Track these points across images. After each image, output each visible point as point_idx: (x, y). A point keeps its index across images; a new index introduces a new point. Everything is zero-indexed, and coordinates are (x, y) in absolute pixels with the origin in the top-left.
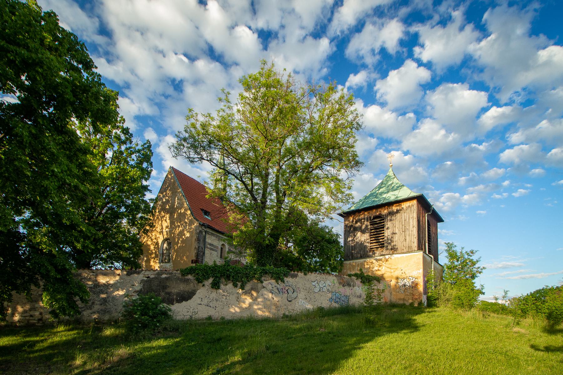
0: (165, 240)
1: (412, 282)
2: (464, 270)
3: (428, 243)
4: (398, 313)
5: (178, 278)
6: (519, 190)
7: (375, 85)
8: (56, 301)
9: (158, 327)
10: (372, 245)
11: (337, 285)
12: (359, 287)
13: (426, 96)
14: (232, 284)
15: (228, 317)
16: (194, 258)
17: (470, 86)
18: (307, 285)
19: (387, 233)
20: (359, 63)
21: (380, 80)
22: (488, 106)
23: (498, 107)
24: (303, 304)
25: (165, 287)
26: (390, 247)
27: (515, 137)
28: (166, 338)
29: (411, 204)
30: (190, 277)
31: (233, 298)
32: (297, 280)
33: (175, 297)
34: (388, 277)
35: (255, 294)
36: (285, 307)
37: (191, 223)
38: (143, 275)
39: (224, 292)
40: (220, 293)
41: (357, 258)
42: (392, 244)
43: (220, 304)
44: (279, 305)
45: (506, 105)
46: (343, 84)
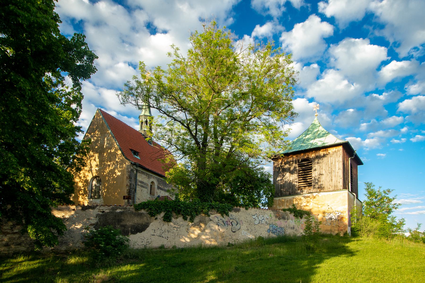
0: (94, 178)
1: (338, 216)
2: (380, 206)
3: (351, 183)
4: (332, 242)
5: (132, 213)
6: (417, 136)
7: (280, 36)
8: (43, 232)
9: (120, 255)
10: (300, 184)
11: (274, 218)
12: (292, 220)
13: (330, 48)
14: (182, 217)
15: (179, 246)
16: (126, 195)
17: (371, 41)
18: (248, 218)
19: (314, 174)
20: (264, 15)
21: (285, 32)
22: (388, 60)
23: (397, 61)
24: (246, 234)
25: (120, 221)
26: (317, 186)
27: (413, 89)
28: (131, 264)
29: (337, 150)
30: (143, 211)
31: (184, 229)
32: (239, 214)
33: (130, 229)
34: (316, 212)
35: (203, 225)
36: (230, 237)
37: (122, 162)
38: (98, 210)
39: (175, 224)
40: (171, 225)
41: (286, 195)
42: (319, 183)
43: (172, 234)
44: (225, 235)
45: (405, 59)
46: (250, 34)
